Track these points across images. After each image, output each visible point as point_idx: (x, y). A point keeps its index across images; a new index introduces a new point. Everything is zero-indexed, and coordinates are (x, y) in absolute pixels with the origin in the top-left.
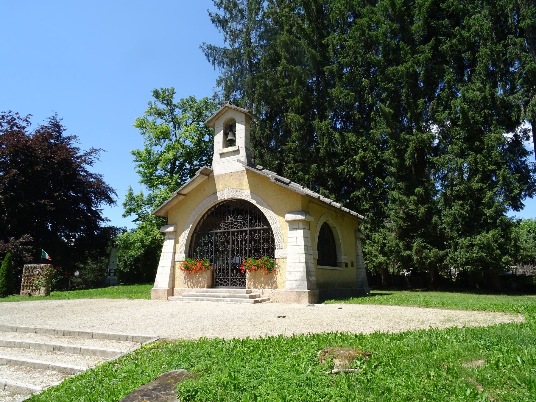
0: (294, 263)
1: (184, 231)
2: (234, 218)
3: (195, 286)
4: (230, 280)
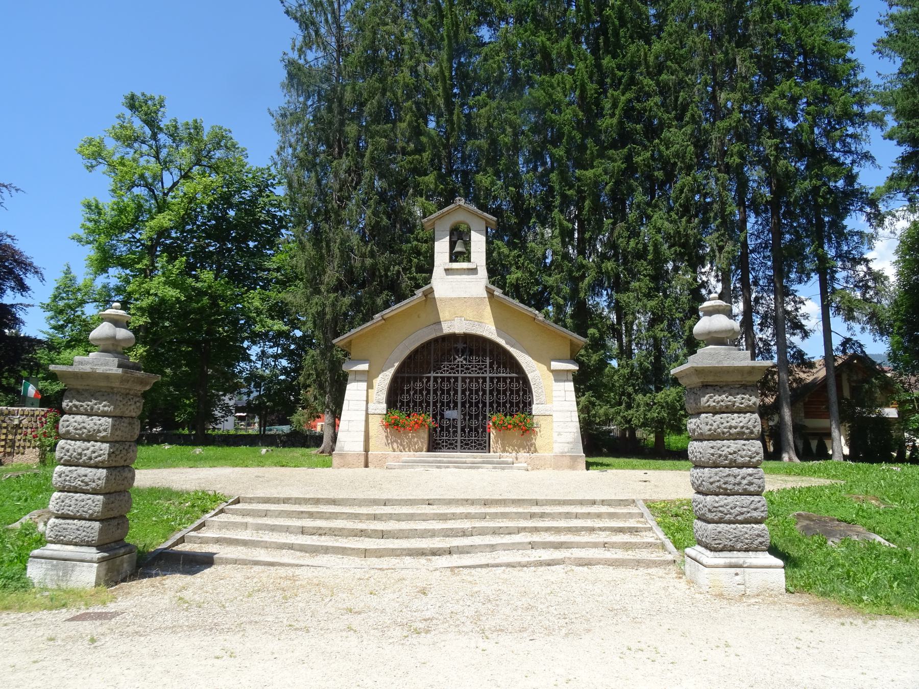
0: (565, 422)
2: (465, 359)
3: (407, 450)
4: (459, 441)
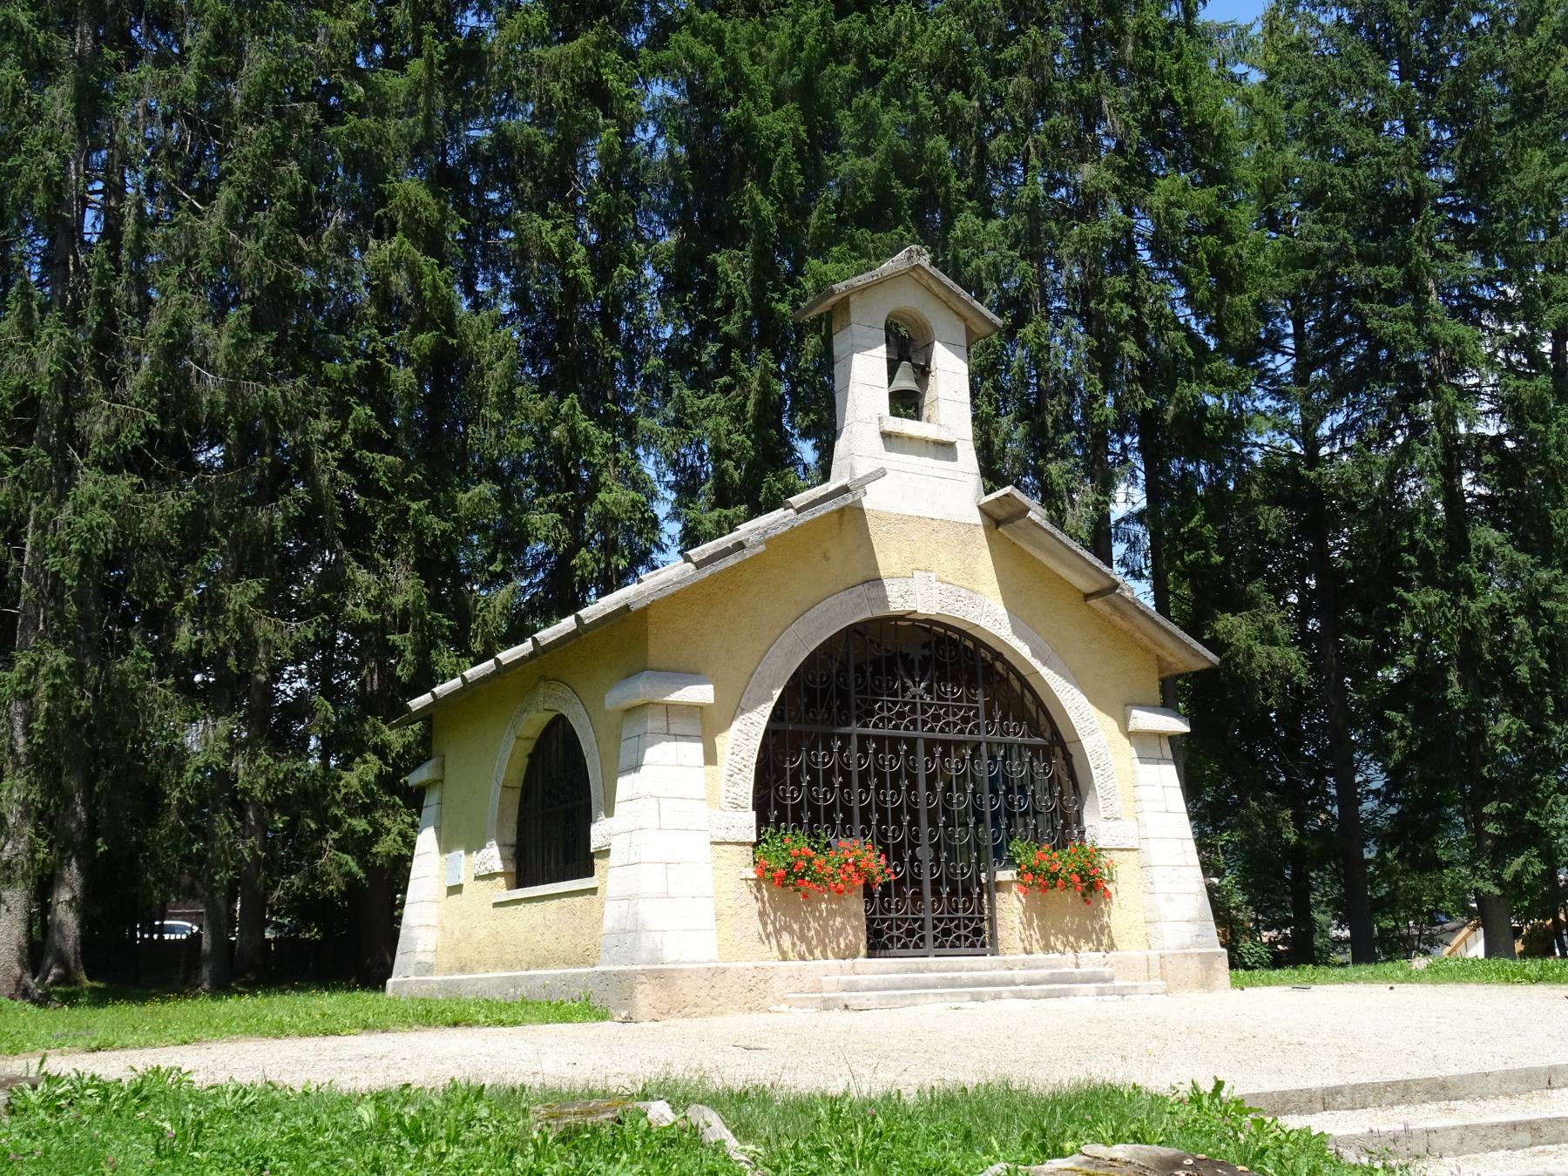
1: (743, 711)
2: (929, 690)
3: (817, 952)
4: (929, 925)
